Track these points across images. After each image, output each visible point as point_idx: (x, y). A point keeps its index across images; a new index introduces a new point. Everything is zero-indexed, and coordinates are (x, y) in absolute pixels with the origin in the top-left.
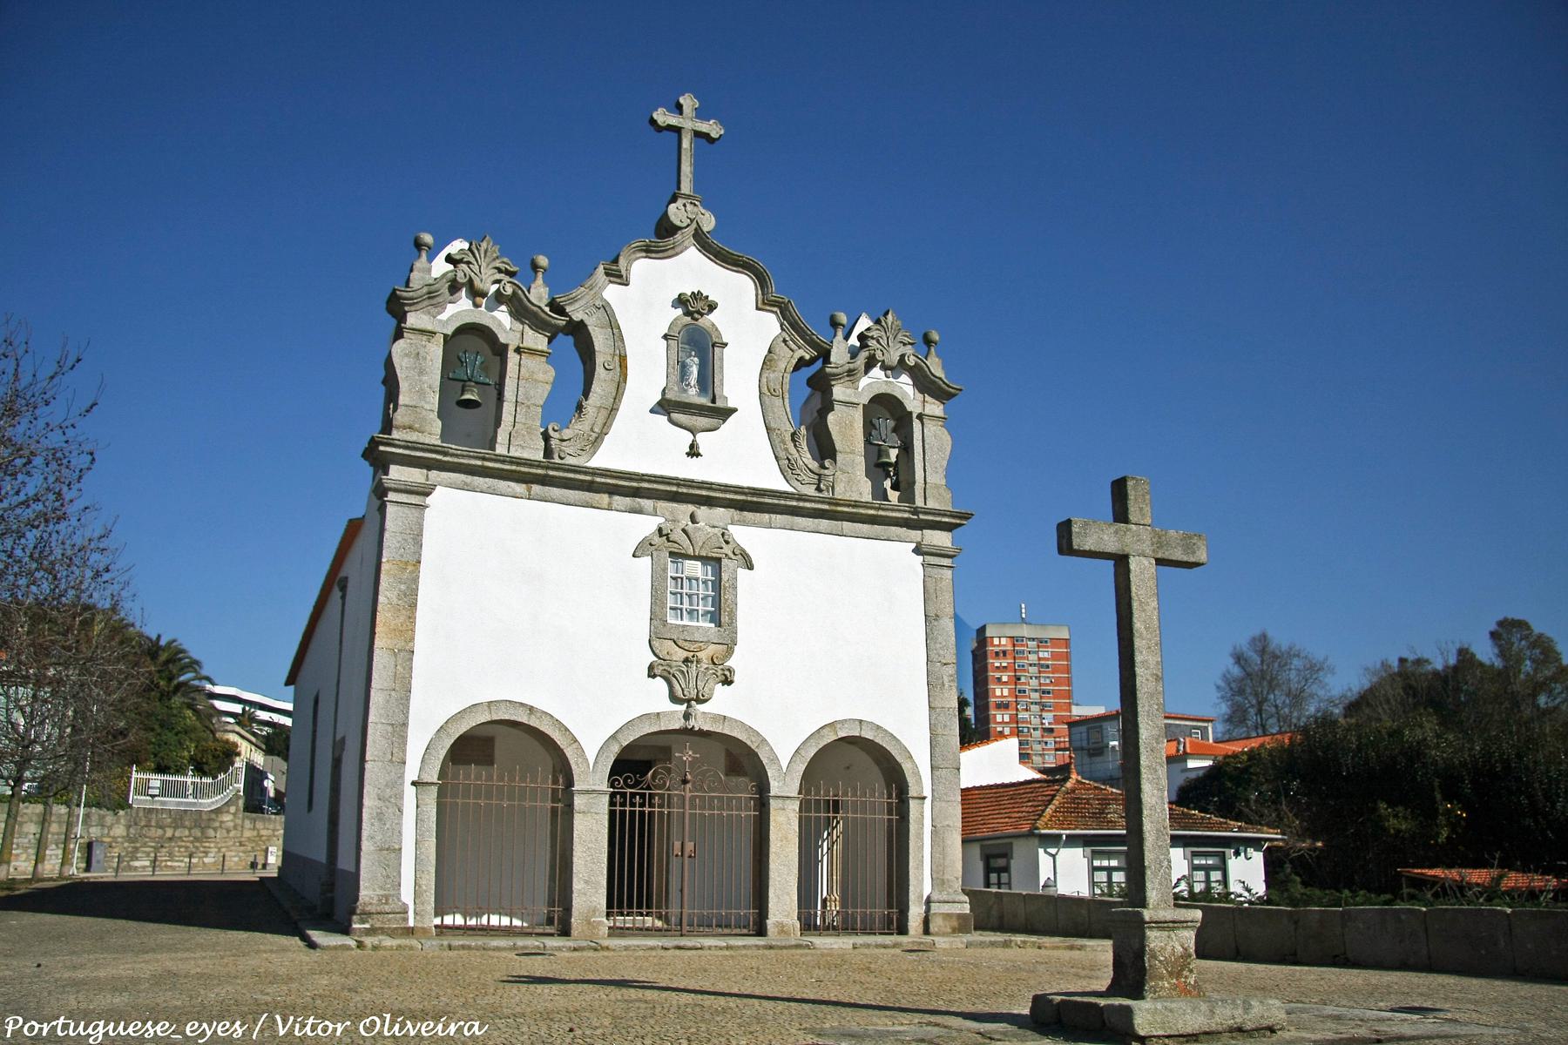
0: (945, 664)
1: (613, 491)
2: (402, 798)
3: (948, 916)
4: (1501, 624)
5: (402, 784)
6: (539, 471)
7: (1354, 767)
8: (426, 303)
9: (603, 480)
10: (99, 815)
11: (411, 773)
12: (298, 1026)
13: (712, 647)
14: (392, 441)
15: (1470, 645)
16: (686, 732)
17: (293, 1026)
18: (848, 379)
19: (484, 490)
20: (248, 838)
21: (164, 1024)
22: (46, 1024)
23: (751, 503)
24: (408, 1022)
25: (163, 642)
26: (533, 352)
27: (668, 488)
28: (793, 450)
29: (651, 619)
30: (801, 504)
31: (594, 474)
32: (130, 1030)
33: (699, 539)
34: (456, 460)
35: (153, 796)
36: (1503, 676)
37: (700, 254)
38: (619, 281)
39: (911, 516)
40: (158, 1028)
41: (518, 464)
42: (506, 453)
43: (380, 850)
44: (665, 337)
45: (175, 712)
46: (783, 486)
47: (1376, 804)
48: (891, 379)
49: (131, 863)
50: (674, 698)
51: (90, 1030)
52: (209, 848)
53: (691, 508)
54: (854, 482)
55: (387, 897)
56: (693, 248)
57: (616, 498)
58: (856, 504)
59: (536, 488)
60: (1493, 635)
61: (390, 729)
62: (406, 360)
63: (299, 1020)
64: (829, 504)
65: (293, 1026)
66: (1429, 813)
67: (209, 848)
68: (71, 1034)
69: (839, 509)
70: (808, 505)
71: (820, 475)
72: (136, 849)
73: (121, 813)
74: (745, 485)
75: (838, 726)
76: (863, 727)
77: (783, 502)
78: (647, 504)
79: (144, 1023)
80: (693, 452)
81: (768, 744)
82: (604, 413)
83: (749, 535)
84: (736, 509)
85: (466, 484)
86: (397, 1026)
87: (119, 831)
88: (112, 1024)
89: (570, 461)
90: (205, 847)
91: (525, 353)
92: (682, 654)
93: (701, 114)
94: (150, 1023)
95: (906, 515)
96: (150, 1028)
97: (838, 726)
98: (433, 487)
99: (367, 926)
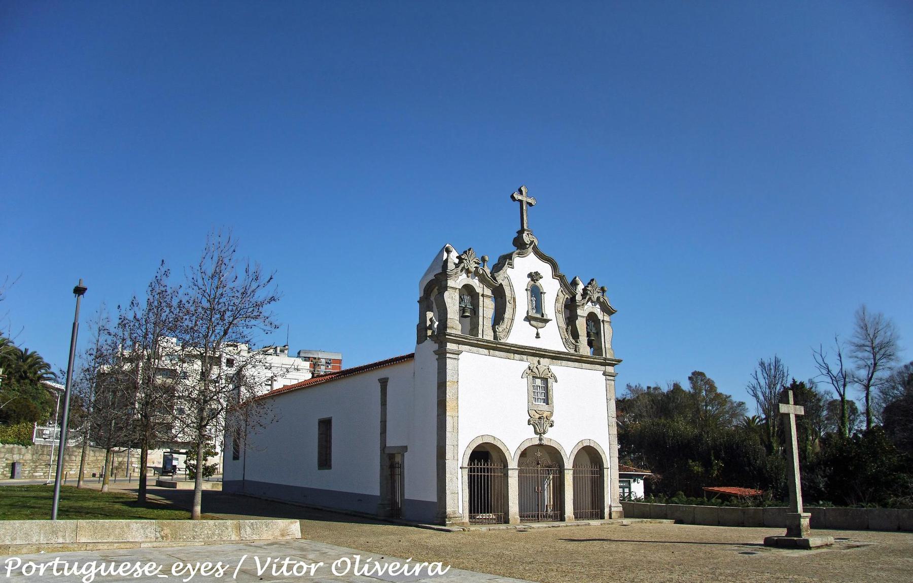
1: (515, 352)
4: (694, 374)
7: (672, 444)
10: (18, 448)
12: (274, 566)
15: (680, 383)
16: (540, 445)
17: (270, 567)
20: (92, 461)
22: (42, 565)
23: (556, 357)
24: (377, 563)
25: (29, 353)
26: (488, 296)
32: (121, 570)
33: (541, 370)
35: (45, 439)
36: (694, 396)
40: (146, 568)
41: (488, 343)
42: (482, 338)
44: (526, 290)
45: (40, 391)
46: (564, 350)
47: (687, 460)
49: (34, 474)
50: (536, 433)
51: (83, 570)
52: (73, 466)
53: (538, 359)
54: (585, 350)
60: (690, 378)
63: (276, 561)
64: (580, 357)
65: (270, 567)
66: (707, 464)
67: (73, 466)
68: (66, 573)
69: (583, 359)
70: (574, 357)
71: (576, 345)
72: (37, 466)
73: (29, 447)
78: (525, 357)
79: (133, 564)
80: (538, 336)
82: (510, 321)
83: (559, 369)
86: (366, 567)
87: (28, 456)
88: (104, 565)
90: (71, 465)
94: (139, 564)
96: (139, 569)
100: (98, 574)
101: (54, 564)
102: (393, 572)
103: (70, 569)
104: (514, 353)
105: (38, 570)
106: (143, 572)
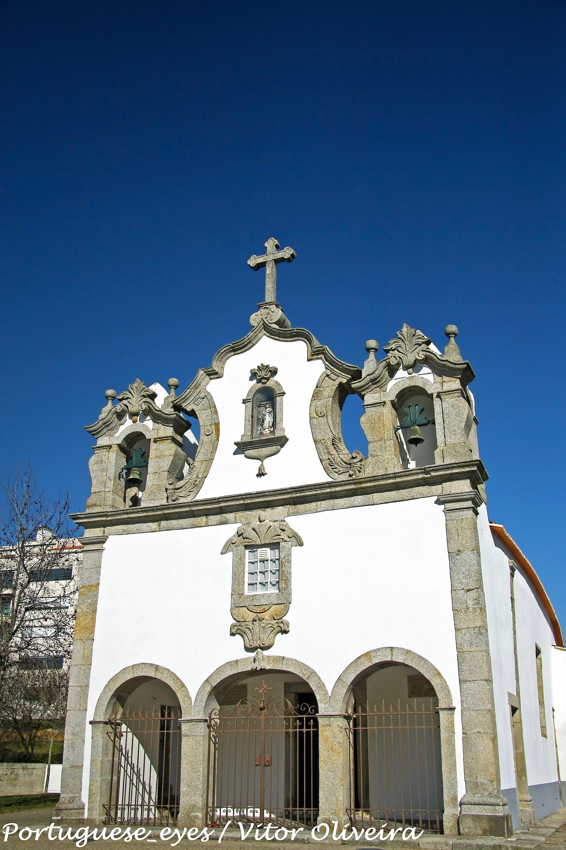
0: (468, 590)
1: (207, 513)
2: (84, 733)
3: (477, 818)
5: (85, 724)
6: (159, 513)
8: (105, 430)
9: (197, 508)
11: (90, 716)
13: (274, 607)
14: (78, 516)
16: (254, 673)
18: (374, 386)
19: (135, 531)
21: (117, 830)
27: (238, 503)
28: (333, 452)
29: (232, 594)
30: (333, 490)
31: (189, 506)
34: (113, 518)
37: (269, 339)
38: (216, 376)
39: (425, 476)
40: (136, 833)
43: (71, 767)
48: (414, 374)
51: (77, 836)
55: (73, 798)
56: (265, 337)
57: (211, 517)
58: (386, 477)
59: (163, 523)
61: (79, 689)
62: (95, 466)
64: (355, 484)
68: (61, 838)
69: (363, 485)
74: (288, 486)
75: (373, 655)
76: (394, 653)
77: (319, 492)
78: (230, 516)
80: (261, 474)
81: (317, 675)
84: (290, 504)
85: (124, 531)
89: (182, 500)
91: (158, 441)
92: (252, 616)
93: (263, 251)
95: (420, 476)
97: (373, 655)
98: (106, 538)
99: (59, 818)
100: (90, 840)
101: (49, 829)
102: (192, 837)
103: (64, 833)
104: (207, 515)
105: (34, 835)
106: (133, 837)
